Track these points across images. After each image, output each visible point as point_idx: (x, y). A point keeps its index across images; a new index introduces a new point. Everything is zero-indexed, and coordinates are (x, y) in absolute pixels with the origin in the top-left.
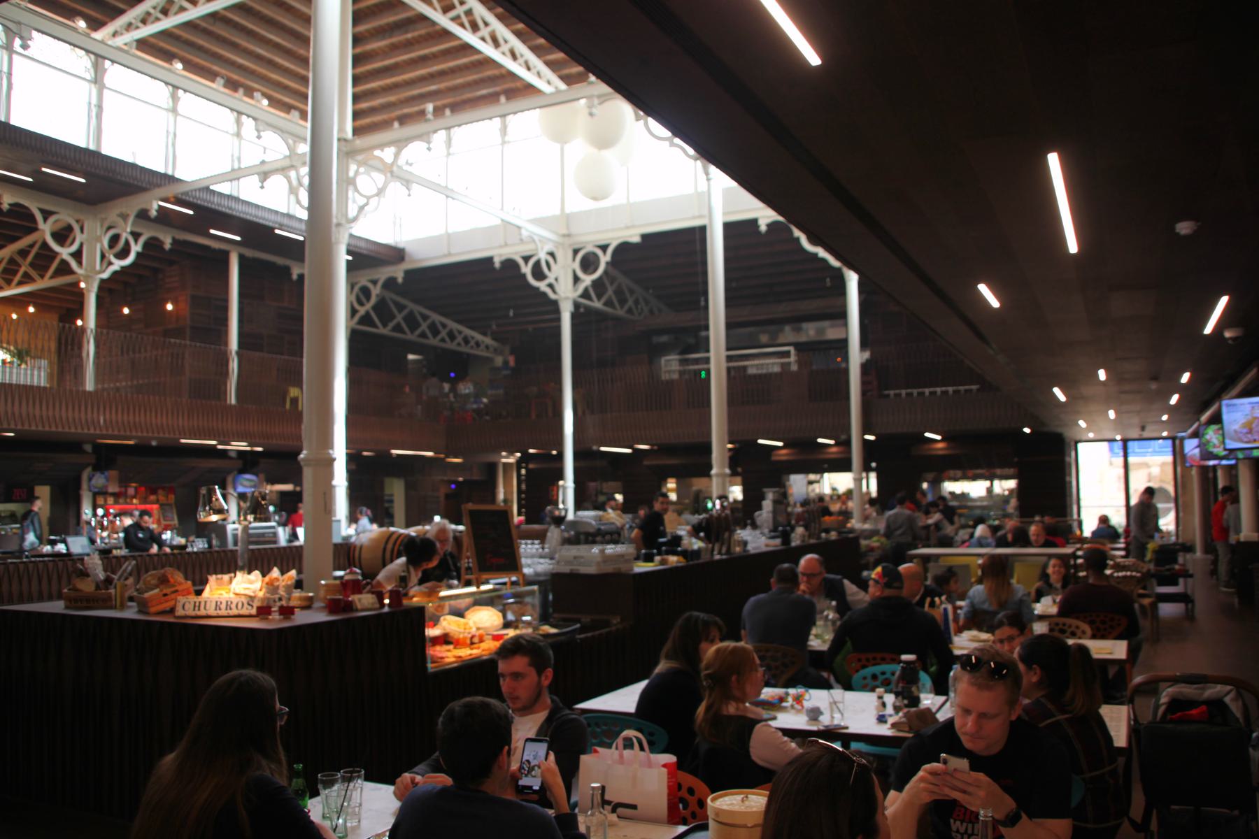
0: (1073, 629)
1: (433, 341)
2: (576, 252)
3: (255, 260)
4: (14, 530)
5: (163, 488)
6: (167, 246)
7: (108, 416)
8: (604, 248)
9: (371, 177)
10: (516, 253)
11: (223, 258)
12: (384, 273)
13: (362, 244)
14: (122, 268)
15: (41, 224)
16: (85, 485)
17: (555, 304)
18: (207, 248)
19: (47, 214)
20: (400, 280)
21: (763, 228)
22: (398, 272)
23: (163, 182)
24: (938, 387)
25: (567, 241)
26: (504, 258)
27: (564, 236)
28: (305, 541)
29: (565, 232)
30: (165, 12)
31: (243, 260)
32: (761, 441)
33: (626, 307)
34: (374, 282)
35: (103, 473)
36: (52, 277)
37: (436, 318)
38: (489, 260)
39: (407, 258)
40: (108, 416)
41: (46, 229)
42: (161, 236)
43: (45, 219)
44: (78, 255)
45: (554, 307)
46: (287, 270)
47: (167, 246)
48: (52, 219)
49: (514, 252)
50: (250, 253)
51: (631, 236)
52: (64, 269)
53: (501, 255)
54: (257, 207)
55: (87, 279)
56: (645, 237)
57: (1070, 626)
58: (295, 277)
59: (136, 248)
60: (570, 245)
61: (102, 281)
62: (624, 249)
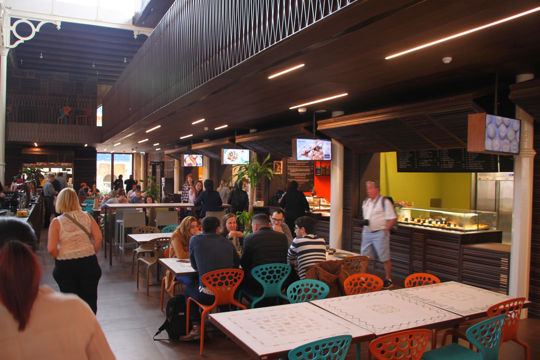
2: (13, 20)
8: (36, 23)
62: (49, 27)
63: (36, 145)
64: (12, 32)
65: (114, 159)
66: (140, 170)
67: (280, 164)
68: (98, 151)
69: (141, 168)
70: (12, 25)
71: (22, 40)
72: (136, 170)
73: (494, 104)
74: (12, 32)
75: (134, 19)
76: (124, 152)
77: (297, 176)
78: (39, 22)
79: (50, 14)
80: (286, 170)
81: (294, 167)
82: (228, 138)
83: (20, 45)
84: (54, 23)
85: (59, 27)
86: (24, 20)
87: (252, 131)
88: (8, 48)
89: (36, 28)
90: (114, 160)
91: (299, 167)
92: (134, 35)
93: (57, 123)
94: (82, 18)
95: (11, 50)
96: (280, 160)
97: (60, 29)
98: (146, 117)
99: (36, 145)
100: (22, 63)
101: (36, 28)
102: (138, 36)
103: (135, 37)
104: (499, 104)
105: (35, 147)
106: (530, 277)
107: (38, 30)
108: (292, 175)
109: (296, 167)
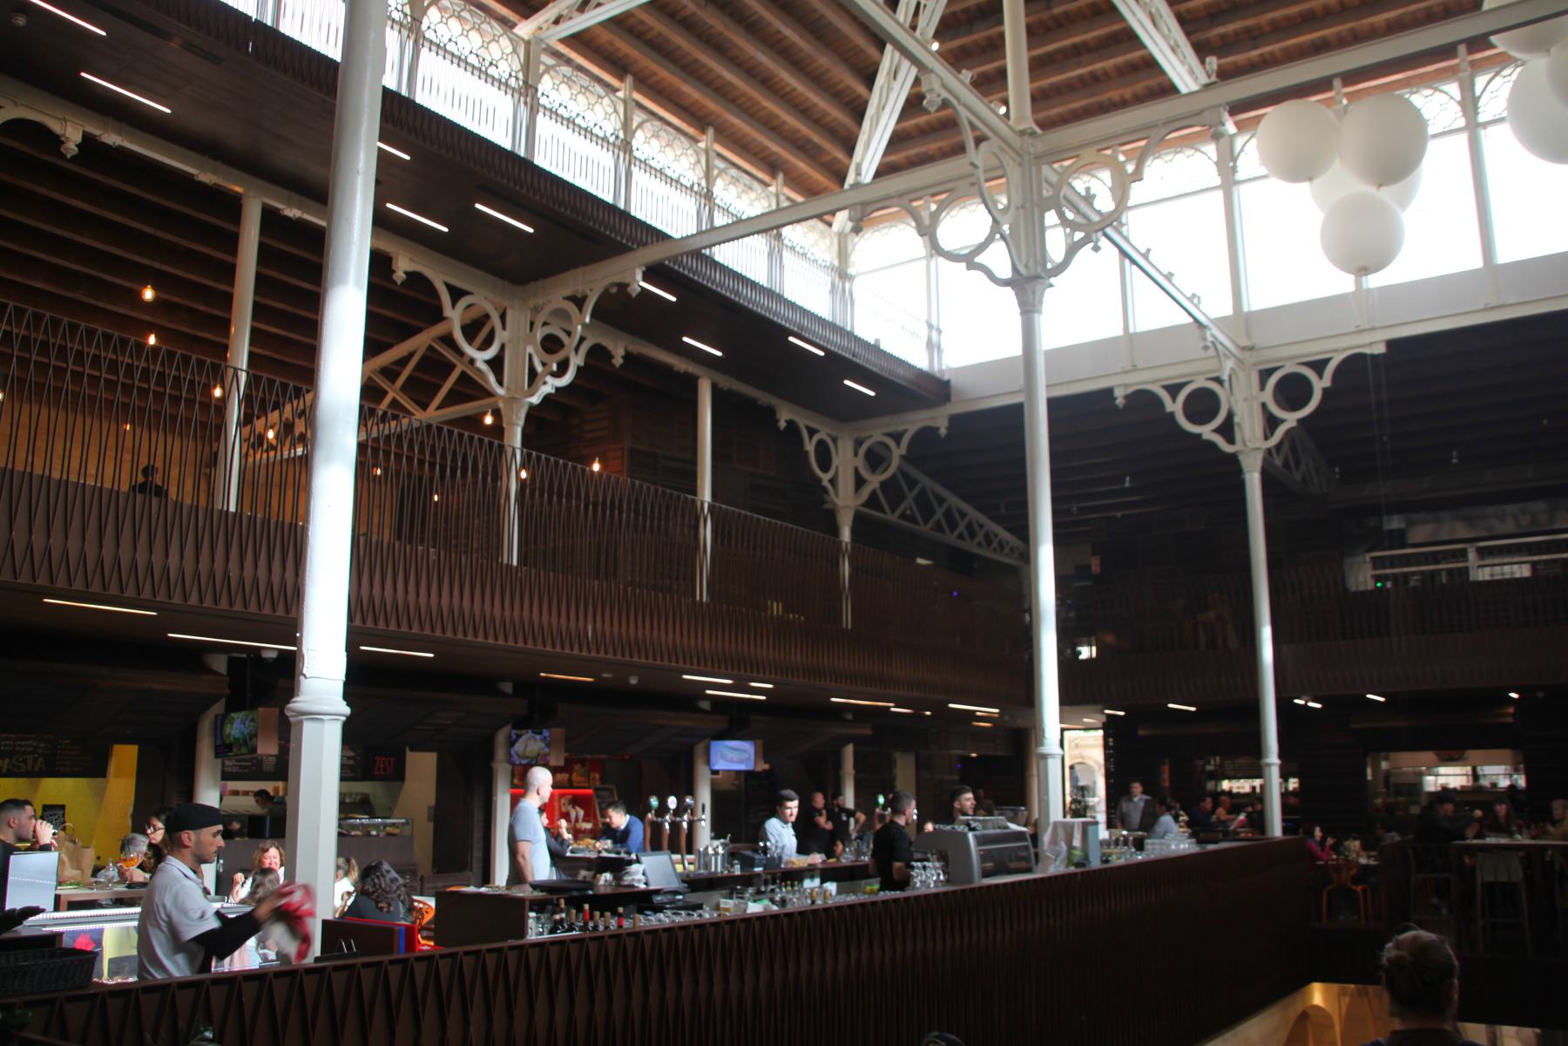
1: (950, 538)
2: (1265, 374)
3: (730, 392)
4: (389, 829)
5: (583, 762)
6: (618, 361)
7: (599, 625)
8: (1319, 366)
9: (1202, 152)
10: (1154, 382)
11: (691, 383)
12: (913, 422)
13: (901, 371)
14: (557, 389)
15: (448, 311)
16: (500, 753)
17: (1233, 459)
18: (667, 370)
19: (456, 294)
20: (943, 431)
21: (1120, 402)
22: (939, 419)
23: (650, 240)
25: (1249, 358)
26: (1130, 390)
27: (1244, 349)
29: (1245, 342)
30: (582, 8)
31: (717, 393)
32: (1369, 696)
33: (957, 533)
34: (897, 437)
35: (540, 733)
36: (439, 408)
37: (954, 501)
38: (1108, 393)
39: (953, 398)
40: (599, 625)
41: (455, 316)
42: (608, 343)
43: (454, 303)
44: (496, 364)
46: (770, 413)
47: (618, 361)
48: (463, 302)
49: (1150, 379)
50: (727, 383)
52: (470, 389)
53: (1126, 386)
55: (512, 400)
56: (1391, 344)
58: (782, 425)
59: (576, 361)
60: (1255, 364)
61: (532, 408)
62: (1355, 364)
64: (1264, 406)
70: (1262, 387)
71: (1291, 419)
73: (1293, 784)
74: (1264, 406)
78: (1326, 362)
79: (1216, 359)
83: (1289, 432)
86: (1290, 368)
89: (1320, 375)
92: (1115, 399)
95: (1269, 451)
98: (335, 954)
100: (1455, 461)
104: (1086, 652)
106: (334, 105)
107: (1326, 381)
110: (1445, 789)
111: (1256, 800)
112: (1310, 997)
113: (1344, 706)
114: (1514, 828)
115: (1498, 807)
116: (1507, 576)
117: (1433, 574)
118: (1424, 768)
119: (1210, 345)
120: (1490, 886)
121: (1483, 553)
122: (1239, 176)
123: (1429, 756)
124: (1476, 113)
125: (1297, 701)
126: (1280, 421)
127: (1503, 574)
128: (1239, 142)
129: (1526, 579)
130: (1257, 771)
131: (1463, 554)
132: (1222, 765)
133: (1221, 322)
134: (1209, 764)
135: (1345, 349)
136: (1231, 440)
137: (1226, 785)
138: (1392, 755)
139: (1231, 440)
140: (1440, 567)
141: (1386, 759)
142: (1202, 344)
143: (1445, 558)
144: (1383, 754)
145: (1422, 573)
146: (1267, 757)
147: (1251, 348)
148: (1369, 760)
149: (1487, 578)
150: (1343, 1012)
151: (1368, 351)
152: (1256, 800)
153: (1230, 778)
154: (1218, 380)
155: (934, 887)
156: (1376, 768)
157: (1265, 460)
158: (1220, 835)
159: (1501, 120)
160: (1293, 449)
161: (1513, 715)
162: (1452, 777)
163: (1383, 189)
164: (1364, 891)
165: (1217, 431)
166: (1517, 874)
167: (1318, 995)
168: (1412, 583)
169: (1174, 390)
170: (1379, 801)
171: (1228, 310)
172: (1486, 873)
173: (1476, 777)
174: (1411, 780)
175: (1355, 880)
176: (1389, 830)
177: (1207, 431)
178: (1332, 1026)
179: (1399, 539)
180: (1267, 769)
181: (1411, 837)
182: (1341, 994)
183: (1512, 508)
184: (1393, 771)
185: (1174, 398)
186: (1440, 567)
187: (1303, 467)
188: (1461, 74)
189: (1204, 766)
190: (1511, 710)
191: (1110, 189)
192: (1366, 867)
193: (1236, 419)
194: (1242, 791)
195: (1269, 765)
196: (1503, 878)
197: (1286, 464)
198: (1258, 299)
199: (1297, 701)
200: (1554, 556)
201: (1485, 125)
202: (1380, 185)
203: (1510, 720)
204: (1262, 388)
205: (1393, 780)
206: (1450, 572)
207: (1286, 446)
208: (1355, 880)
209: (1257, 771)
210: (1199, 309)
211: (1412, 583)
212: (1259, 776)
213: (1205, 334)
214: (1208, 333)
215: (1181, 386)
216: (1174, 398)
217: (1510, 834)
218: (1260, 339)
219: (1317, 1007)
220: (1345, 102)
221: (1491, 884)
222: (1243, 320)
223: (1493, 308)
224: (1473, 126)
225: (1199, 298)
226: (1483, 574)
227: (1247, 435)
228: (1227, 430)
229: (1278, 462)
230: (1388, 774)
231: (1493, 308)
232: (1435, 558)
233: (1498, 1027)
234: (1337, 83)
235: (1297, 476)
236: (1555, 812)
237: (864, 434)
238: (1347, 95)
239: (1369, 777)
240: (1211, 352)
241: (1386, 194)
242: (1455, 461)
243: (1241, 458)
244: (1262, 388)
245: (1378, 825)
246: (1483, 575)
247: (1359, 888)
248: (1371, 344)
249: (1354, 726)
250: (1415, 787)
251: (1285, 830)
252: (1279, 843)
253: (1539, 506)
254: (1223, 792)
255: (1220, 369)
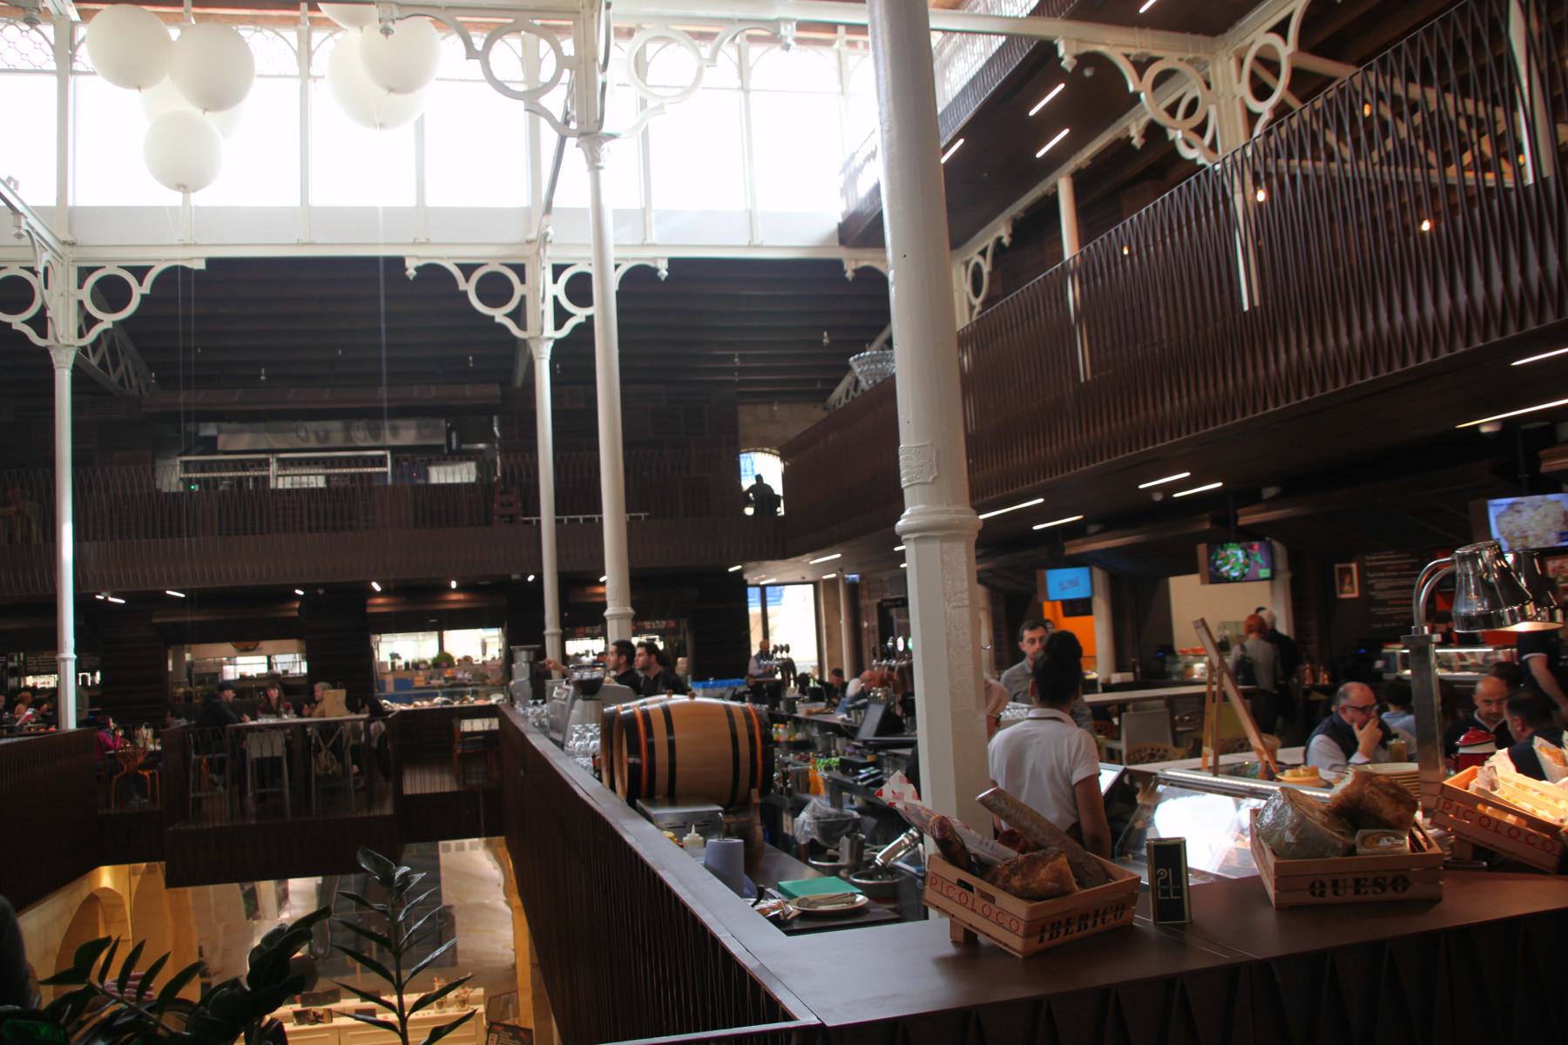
0: (1162, 752)
2: (84, 273)
8: (140, 272)
10: (449, 258)
17: (45, 353)
21: (411, 273)
24: (580, 514)
25: (71, 254)
26: (421, 263)
28: (1542, 652)
32: (168, 592)
38: (399, 262)
45: (42, 363)
51: (191, 259)
54: (878, 79)
56: (211, 262)
57: (1159, 750)
62: (174, 277)
63: (376, 587)
64: (81, 303)
65: (768, 599)
66: (840, 625)
67: (1349, 571)
68: (750, 582)
69: (840, 619)
71: (107, 320)
72: (827, 627)
74: (81, 303)
75: (842, 229)
76: (803, 578)
77: (1392, 600)
78: (149, 268)
79: (31, 249)
80: (1365, 587)
81: (1382, 574)
82: (1206, 516)
84: (651, 264)
85: (664, 273)
86: (111, 270)
87: (1269, 492)
88: (550, 339)
89: (141, 283)
90: (768, 603)
91: (1395, 573)
92: (845, 272)
93: (302, 529)
94: (475, 241)
95: (84, 349)
96: (1350, 561)
97: (666, 278)
99: (376, 587)
101: (141, 283)
102: (856, 271)
103: (849, 274)
105: (374, 593)
107: (146, 289)
108: (1381, 596)
109: (1388, 574)
110: (243, 677)
111: (53, 695)
112: (99, 880)
113: (146, 602)
114: (282, 709)
115: (272, 692)
116: (297, 486)
117: (240, 481)
118: (225, 659)
119: (24, 233)
120: (261, 762)
121: (283, 463)
122: (77, 66)
123: (228, 647)
124: (309, 65)
125: (98, 597)
126: (570, 315)
127: (301, 484)
128: (81, 31)
129: (321, 490)
130: (53, 668)
131: (266, 463)
132: (25, 662)
133: (39, 212)
134: (12, 660)
135: (166, 260)
136: (43, 334)
137: (30, 681)
138: (194, 647)
139: (43, 334)
140: (248, 474)
141: (189, 651)
142: (16, 231)
143: (252, 466)
144: (186, 646)
145: (231, 478)
146: (63, 652)
147: (73, 244)
148: (170, 653)
149: (288, 486)
150: (134, 891)
151: (188, 265)
152: (53, 695)
153: (35, 674)
154: (31, 270)
155: (1436, 654)
156: (178, 660)
157: (77, 357)
158: (5, 732)
159: (261, 76)
160: (112, 351)
161: (299, 610)
162: (251, 665)
163: (207, 113)
164: (152, 775)
165: (509, 315)
166: (279, 751)
167: (106, 877)
168: (221, 488)
169: (468, 269)
170: (182, 690)
171: (50, 200)
172: (256, 750)
173: (270, 666)
174: (213, 669)
175: (145, 766)
176: (179, 717)
177: (500, 315)
178: (122, 905)
179: (210, 445)
180: (62, 664)
181: (194, 722)
182: (133, 873)
183: (312, 425)
184: (197, 662)
185: (467, 279)
186: (248, 474)
187: (122, 368)
188: (300, 26)
189: (6, 663)
190: (297, 605)
191: (520, 59)
192: (155, 753)
193: (49, 314)
194: (47, 686)
195: (65, 660)
196: (267, 754)
197: (103, 365)
198: (83, 195)
199: (98, 597)
200: (345, 471)
201: (315, 78)
202: (206, 110)
203: (296, 614)
204: (80, 286)
205: (196, 670)
206: (256, 479)
207: (104, 347)
208: (145, 766)
209: (53, 668)
210: (15, 195)
211: (221, 488)
212: (54, 671)
213: (19, 221)
214: (23, 221)
215: (476, 267)
216: (467, 279)
217: (278, 715)
218: (82, 237)
219: (106, 889)
220: (193, 21)
221: (259, 760)
222: (64, 214)
223: (304, 244)
224: (305, 75)
225: (16, 184)
226: (284, 482)
227: (60, 330)
228: (518, 316)
229: (94, 361)
230: (191, 665)
231: (304, 244)
232: (243, 465)
233: (256, 883)
234: (841, 29)
235: (114, 378)
236: (316, 693)
237: (968, 258)
238: (195, 15)
239: (170, 669)
240: (26, 241)
241: (211, 119)
242: (263, 378)
243: (532, 344)
244: (80, 286)
245: (169, 714)
246: (284, 483)
247: (146, 774)
248: (192, 259)
249: (155, 620)
250: (216, 674)
251: (79, 724)
252: (70, 735)
253: (335, 426)
254: (27, 688)
255: (35, 260)
